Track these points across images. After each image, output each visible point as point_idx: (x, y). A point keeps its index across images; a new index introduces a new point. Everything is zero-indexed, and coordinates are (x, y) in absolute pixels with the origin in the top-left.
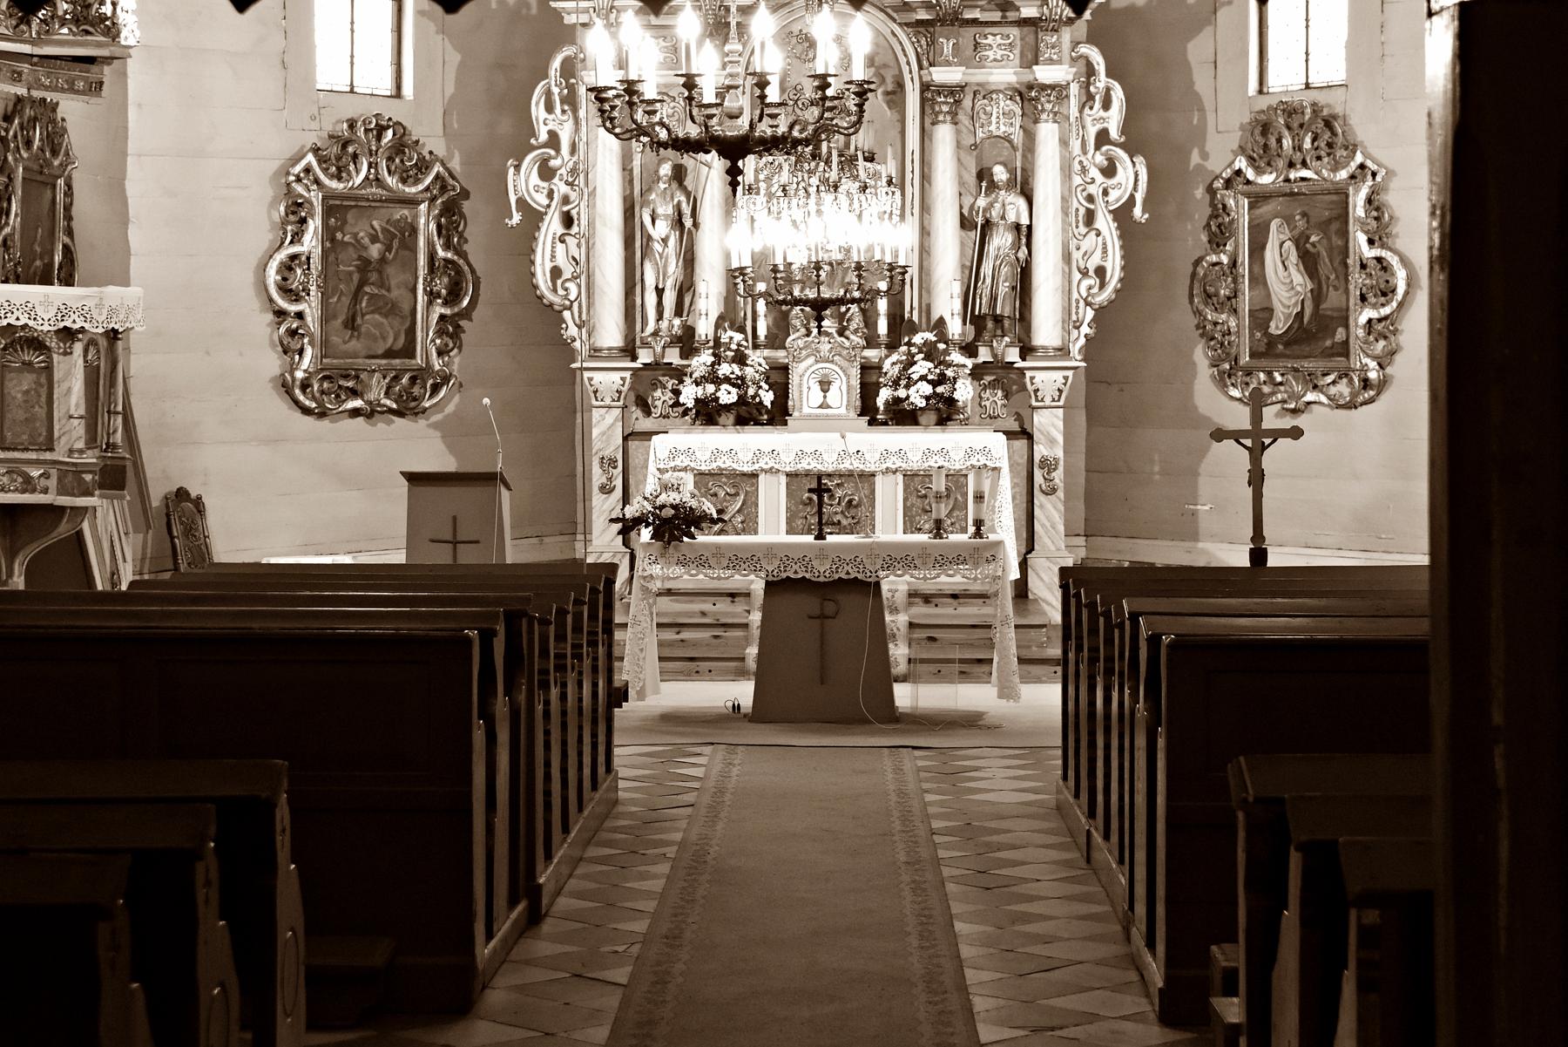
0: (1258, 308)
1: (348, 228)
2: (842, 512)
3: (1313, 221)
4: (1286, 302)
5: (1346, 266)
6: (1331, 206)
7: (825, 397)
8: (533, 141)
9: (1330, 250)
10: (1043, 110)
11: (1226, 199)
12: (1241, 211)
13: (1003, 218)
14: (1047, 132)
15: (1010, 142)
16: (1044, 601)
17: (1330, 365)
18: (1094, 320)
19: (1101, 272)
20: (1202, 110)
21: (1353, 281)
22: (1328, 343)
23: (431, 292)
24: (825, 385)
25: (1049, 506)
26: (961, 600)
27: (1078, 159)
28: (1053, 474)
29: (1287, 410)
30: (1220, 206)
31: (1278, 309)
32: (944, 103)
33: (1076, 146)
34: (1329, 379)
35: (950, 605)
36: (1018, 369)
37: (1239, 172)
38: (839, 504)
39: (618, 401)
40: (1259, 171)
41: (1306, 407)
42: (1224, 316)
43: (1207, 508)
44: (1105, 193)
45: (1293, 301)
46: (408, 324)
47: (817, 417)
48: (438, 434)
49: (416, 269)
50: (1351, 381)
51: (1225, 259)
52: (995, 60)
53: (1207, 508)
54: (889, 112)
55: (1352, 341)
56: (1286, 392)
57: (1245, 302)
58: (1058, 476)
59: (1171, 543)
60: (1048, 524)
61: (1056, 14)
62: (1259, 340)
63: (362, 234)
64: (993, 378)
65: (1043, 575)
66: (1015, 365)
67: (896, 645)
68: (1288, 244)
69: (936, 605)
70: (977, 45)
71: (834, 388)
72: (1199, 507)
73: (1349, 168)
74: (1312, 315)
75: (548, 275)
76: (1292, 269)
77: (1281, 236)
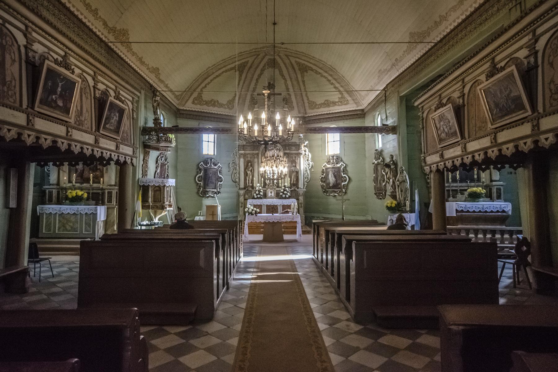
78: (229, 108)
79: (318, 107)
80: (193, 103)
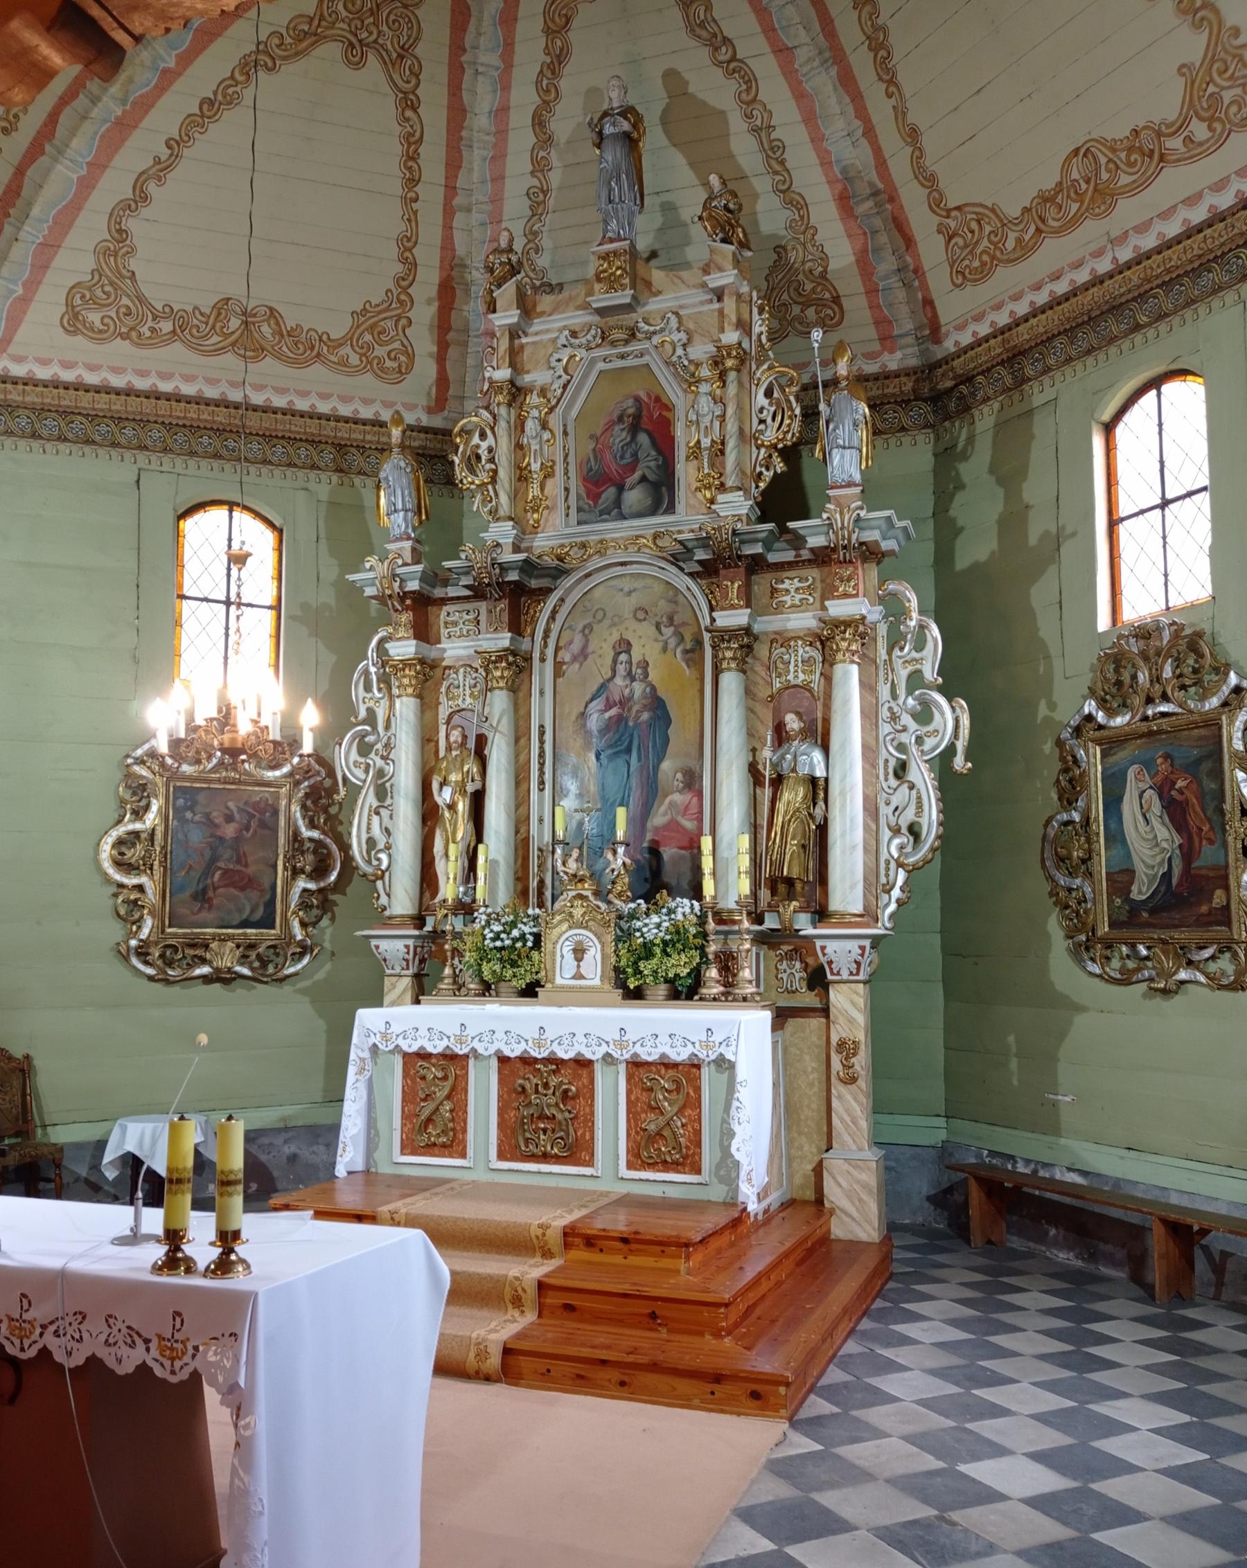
0: (1117, 869)
1: (198, 808)
2: (557, 1105)
3: (1177, 762)
4: (1150, 862)
5: (1222, 813)
6: (1199, 743)
7: (579, 966)
8: (353, 719)
9: (1201, 797)
10: (838, 650)
11: (1076, 749)
12: (1092, 760)
13: (794, 770)
14: (849, 677)
15: (810, 690)
16: (843, 1211)
17: (1207, 935)
18: (906, 883)
19: (914, 831)
20: (1047, 657)
21: (1232, 831)
22: (1204, 909)
23: (294, 868)
24: (579, 953)
25: (849, 1097)
26: (634, 1246)
27: (887, 705)
28: (853, 1060)
29: (1156, 990)
30: (1070, 758)
31: (1140, 868)
32: (727, 648)
33: (884, 691)
34: (1207, 953)
35: (618, 1251)
36: (805, 937)
37: (1090, 718)
38: (554, 1094)
39: (408, 968)
40: (1111, 713)
41: (1179, 988)
42: (1078, 881)
43: (1068, 1099)
44: (920, 741)
45: (1158, 859)
46: (268, 897)
47: (571, 989)
48: (307, 999)
49: (277, 847)
50: (1235, 956)
51: (1076, 817)
52: (793, 606)
53: (1068, 1099)
54: (687, 671)
55: (1233, 906)
56: (1154, 968)
57: (1101, 865)
58: (861, 1062)
59: (1030, 1135)
60: (848, 1119)
61: (843, 536)
62: (1119, 908)
63: (215, 814)
64: (791, 948)
65: (841, 1180)
66: (801, 933)
67: (523, 1312)
68: (1149, 792)
69: (601, 1250)
70: (774, 591)
71: (588, 956)
72: (1060, 1097)
73: (1220, 693)
74: (1182, 876)
75: (364, 846)
76: (1155, 822)
77: (1141, 785)
78: (369, 364)
79: (1019, 241)
80: (73, 322)
